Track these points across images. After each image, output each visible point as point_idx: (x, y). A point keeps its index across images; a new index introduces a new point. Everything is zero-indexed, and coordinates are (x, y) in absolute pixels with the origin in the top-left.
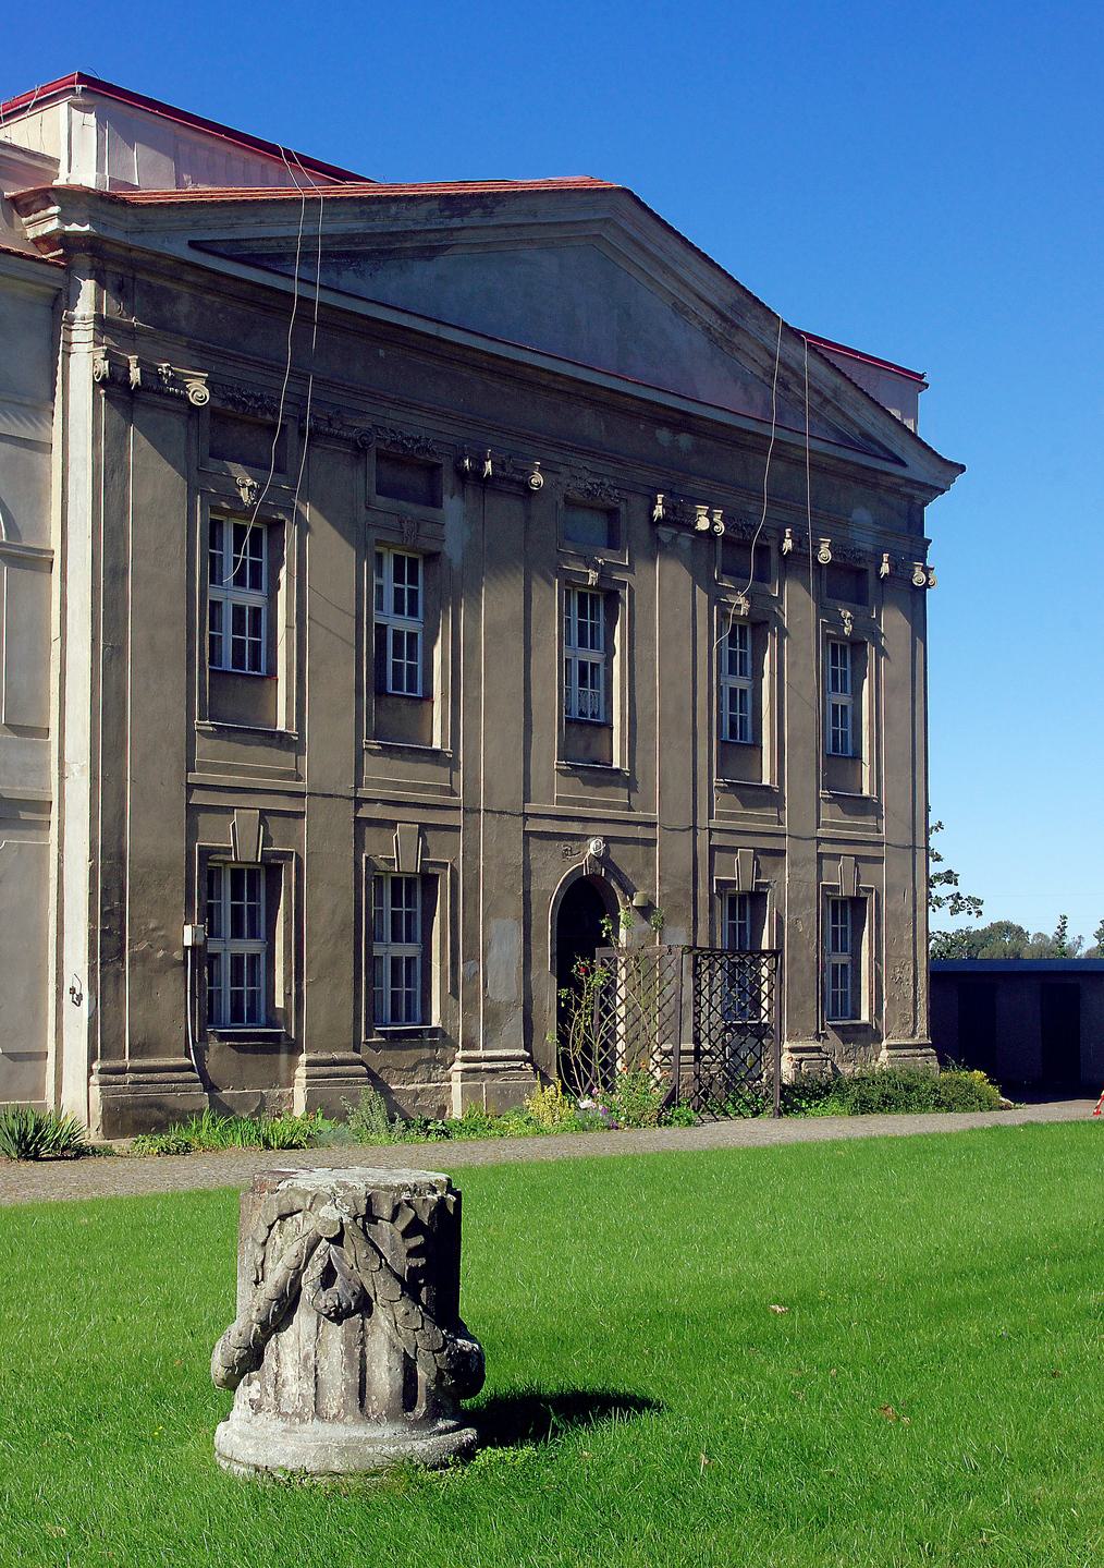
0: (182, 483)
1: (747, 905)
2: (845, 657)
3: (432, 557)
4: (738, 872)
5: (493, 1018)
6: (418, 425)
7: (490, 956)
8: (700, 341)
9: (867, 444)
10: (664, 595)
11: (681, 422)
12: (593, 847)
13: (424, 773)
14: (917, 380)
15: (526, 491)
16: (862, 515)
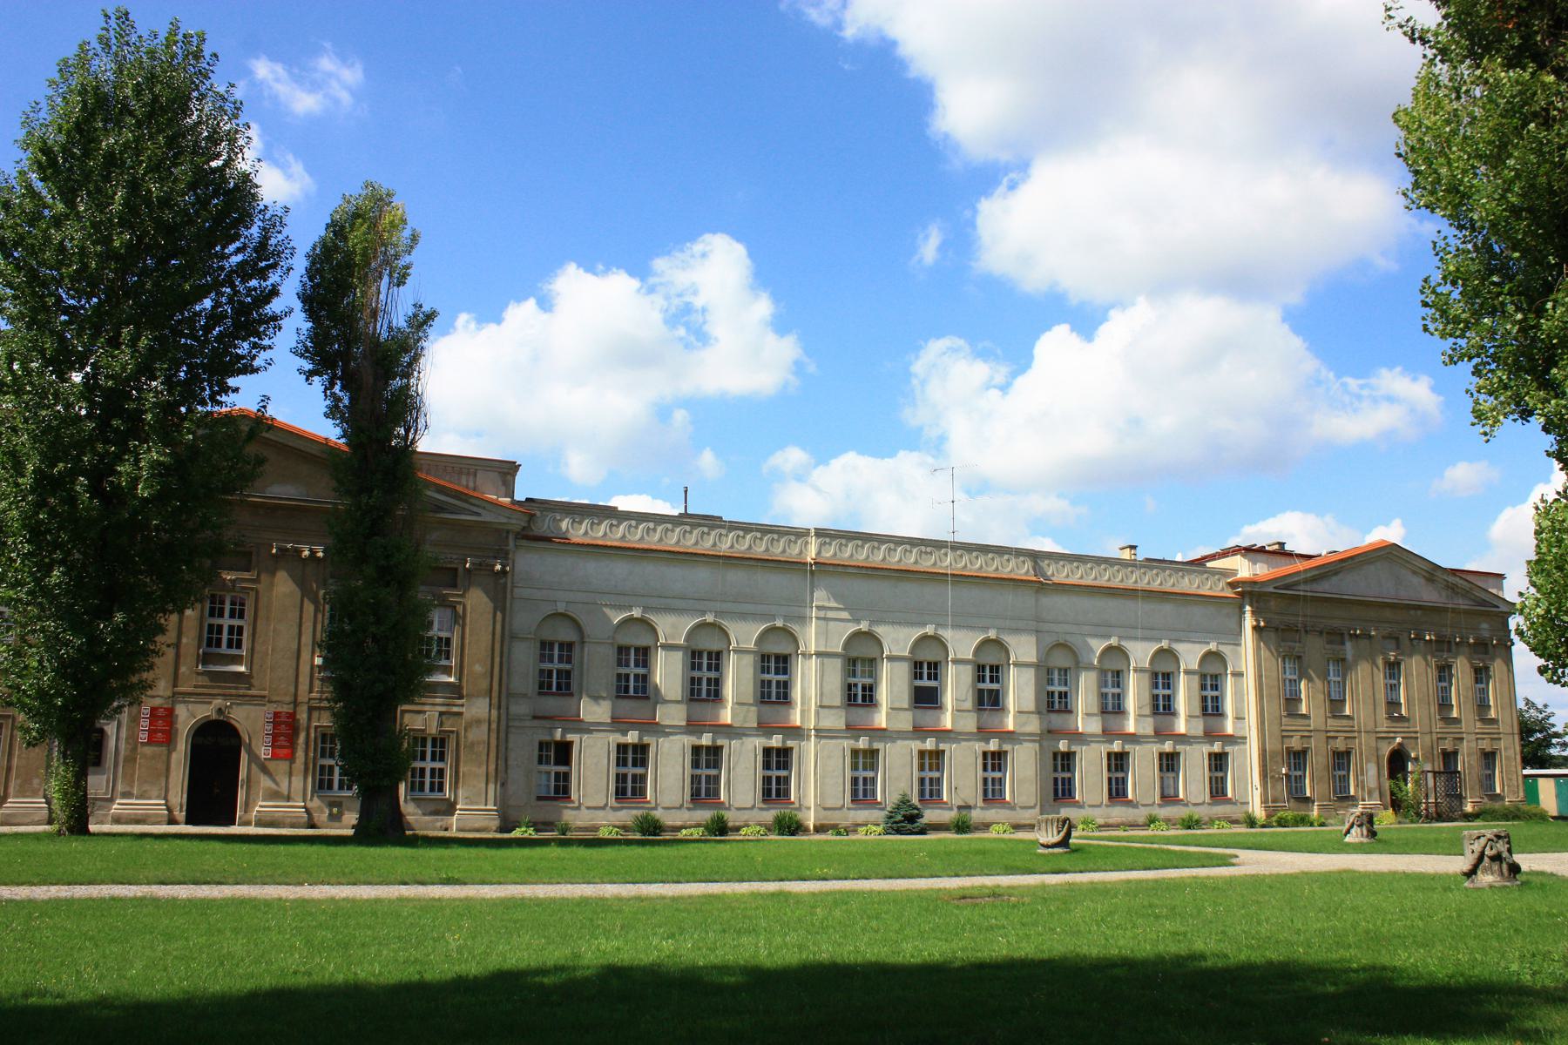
0: (491, 605)
1: (1449, 757)
2: (1481, 674)
3: (1343, 660)
4: (1448, 746)
5: (1370, 793)
6: (1336, 623)
7: (1368, 775)
8: (1423, 581)
9: (1484, 603)
10: (1462, 668)
11: (1419, 607)
12: (1399, 740)
13: (1345, 722)
14: (1501, 577)
15: (1370, 637)
16: (1485, 626)
